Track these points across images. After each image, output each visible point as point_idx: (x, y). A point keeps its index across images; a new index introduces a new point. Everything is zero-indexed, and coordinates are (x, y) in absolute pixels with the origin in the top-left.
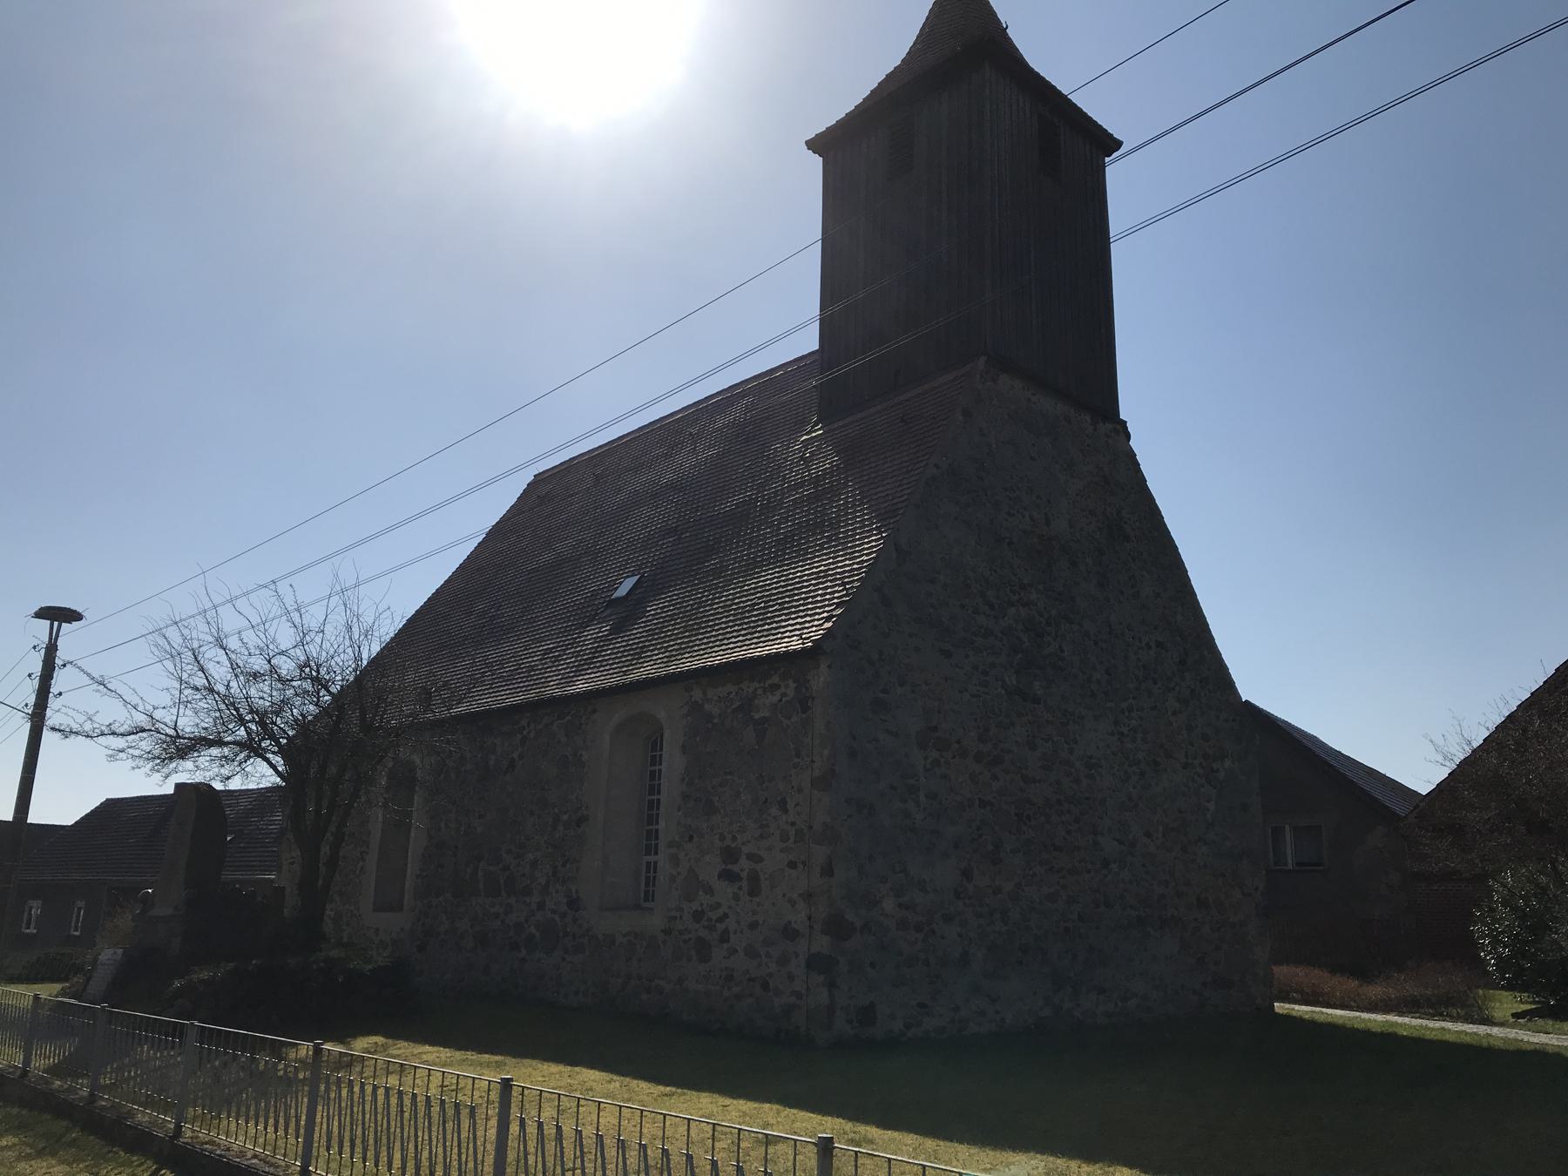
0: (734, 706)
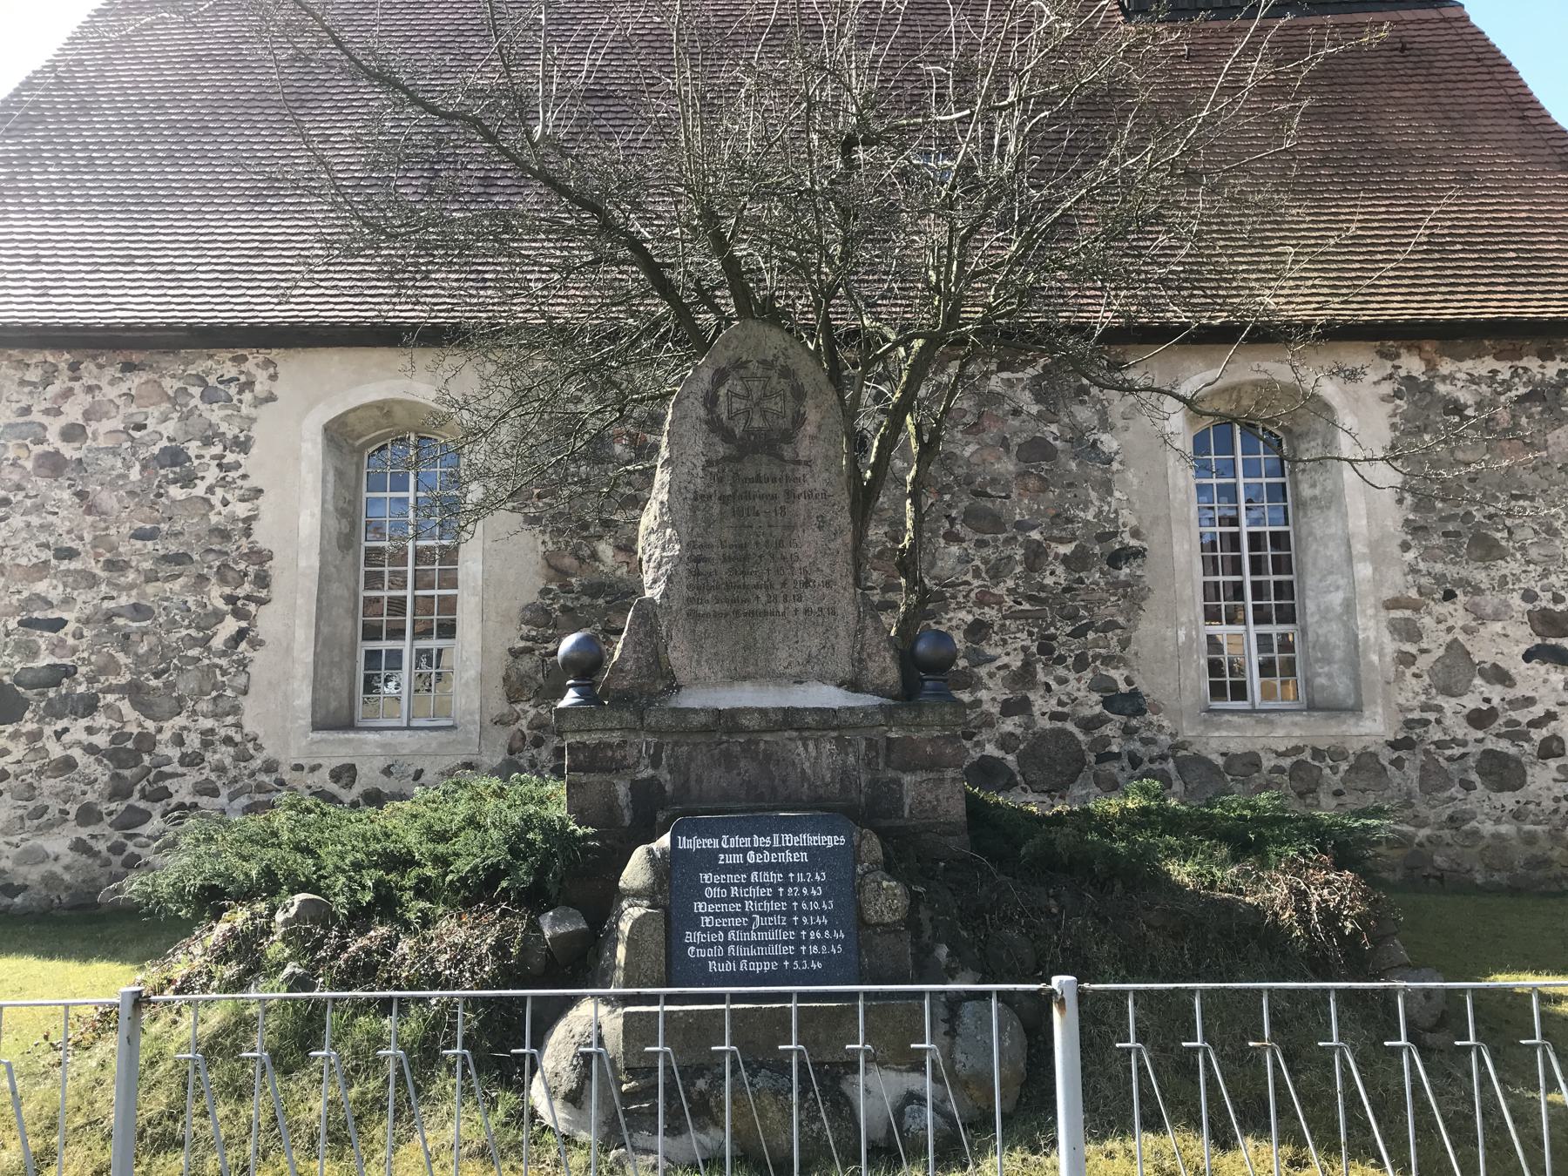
0: (1513, 393)
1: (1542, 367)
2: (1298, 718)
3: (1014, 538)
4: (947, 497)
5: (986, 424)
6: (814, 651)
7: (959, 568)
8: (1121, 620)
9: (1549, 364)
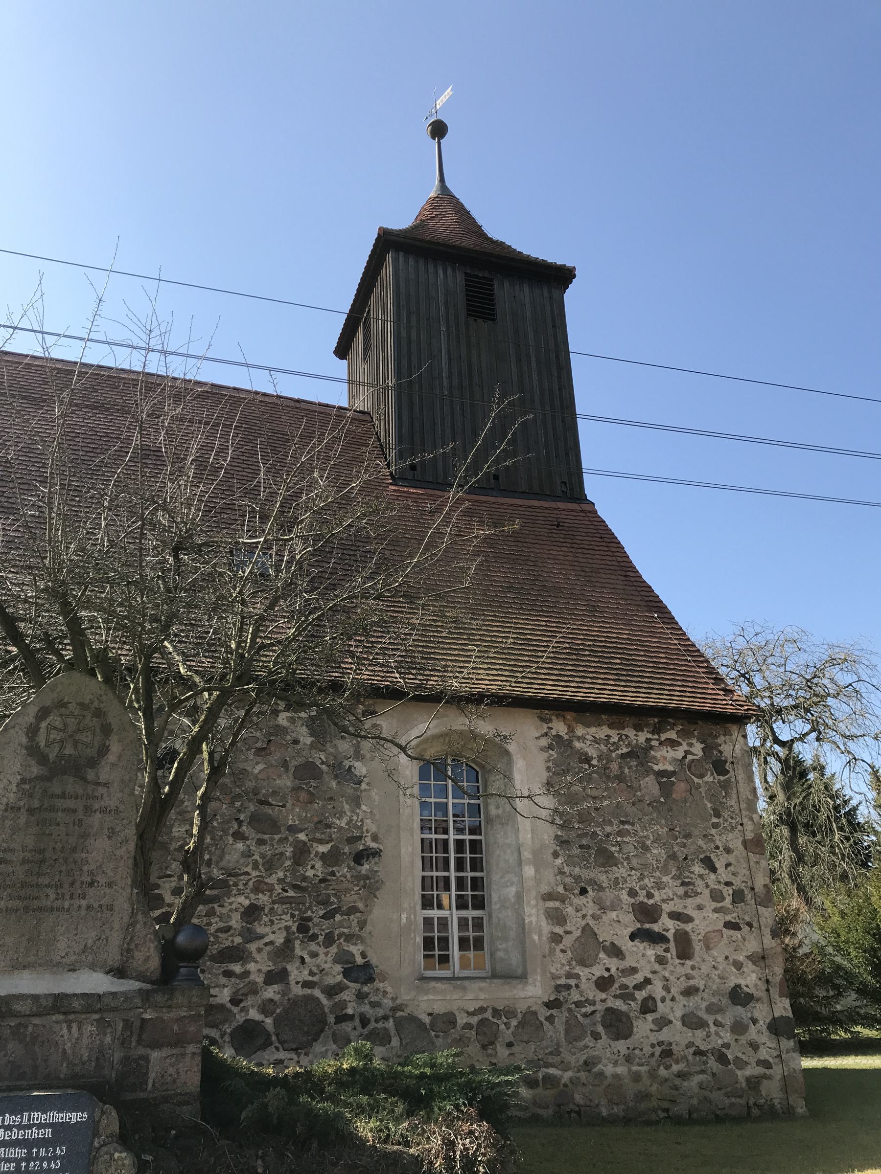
0: (620, 752)
1: (636, 735)
2: (483, 984)
3: (286, 839)
4: (238, 804)
5: (272, 749)
6: (90, 942)
7: (242, 861)
8: (360, 905)
9: (640, 733)
